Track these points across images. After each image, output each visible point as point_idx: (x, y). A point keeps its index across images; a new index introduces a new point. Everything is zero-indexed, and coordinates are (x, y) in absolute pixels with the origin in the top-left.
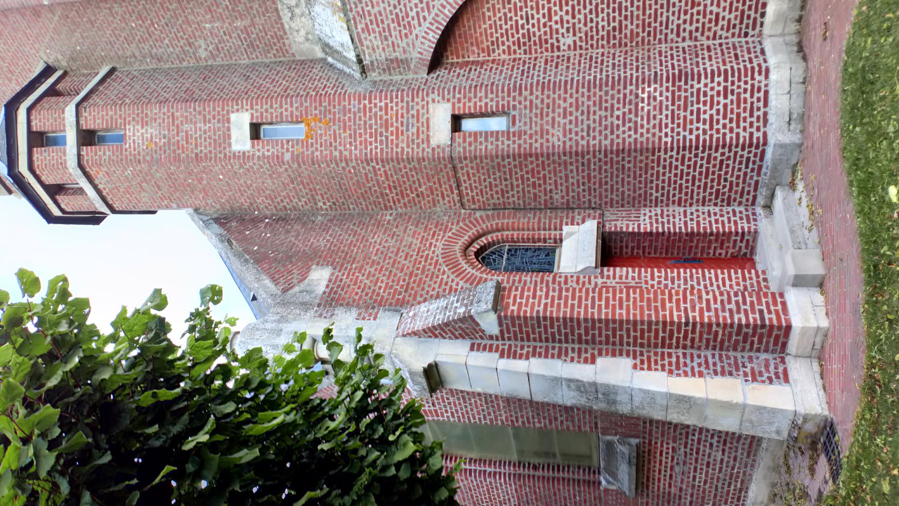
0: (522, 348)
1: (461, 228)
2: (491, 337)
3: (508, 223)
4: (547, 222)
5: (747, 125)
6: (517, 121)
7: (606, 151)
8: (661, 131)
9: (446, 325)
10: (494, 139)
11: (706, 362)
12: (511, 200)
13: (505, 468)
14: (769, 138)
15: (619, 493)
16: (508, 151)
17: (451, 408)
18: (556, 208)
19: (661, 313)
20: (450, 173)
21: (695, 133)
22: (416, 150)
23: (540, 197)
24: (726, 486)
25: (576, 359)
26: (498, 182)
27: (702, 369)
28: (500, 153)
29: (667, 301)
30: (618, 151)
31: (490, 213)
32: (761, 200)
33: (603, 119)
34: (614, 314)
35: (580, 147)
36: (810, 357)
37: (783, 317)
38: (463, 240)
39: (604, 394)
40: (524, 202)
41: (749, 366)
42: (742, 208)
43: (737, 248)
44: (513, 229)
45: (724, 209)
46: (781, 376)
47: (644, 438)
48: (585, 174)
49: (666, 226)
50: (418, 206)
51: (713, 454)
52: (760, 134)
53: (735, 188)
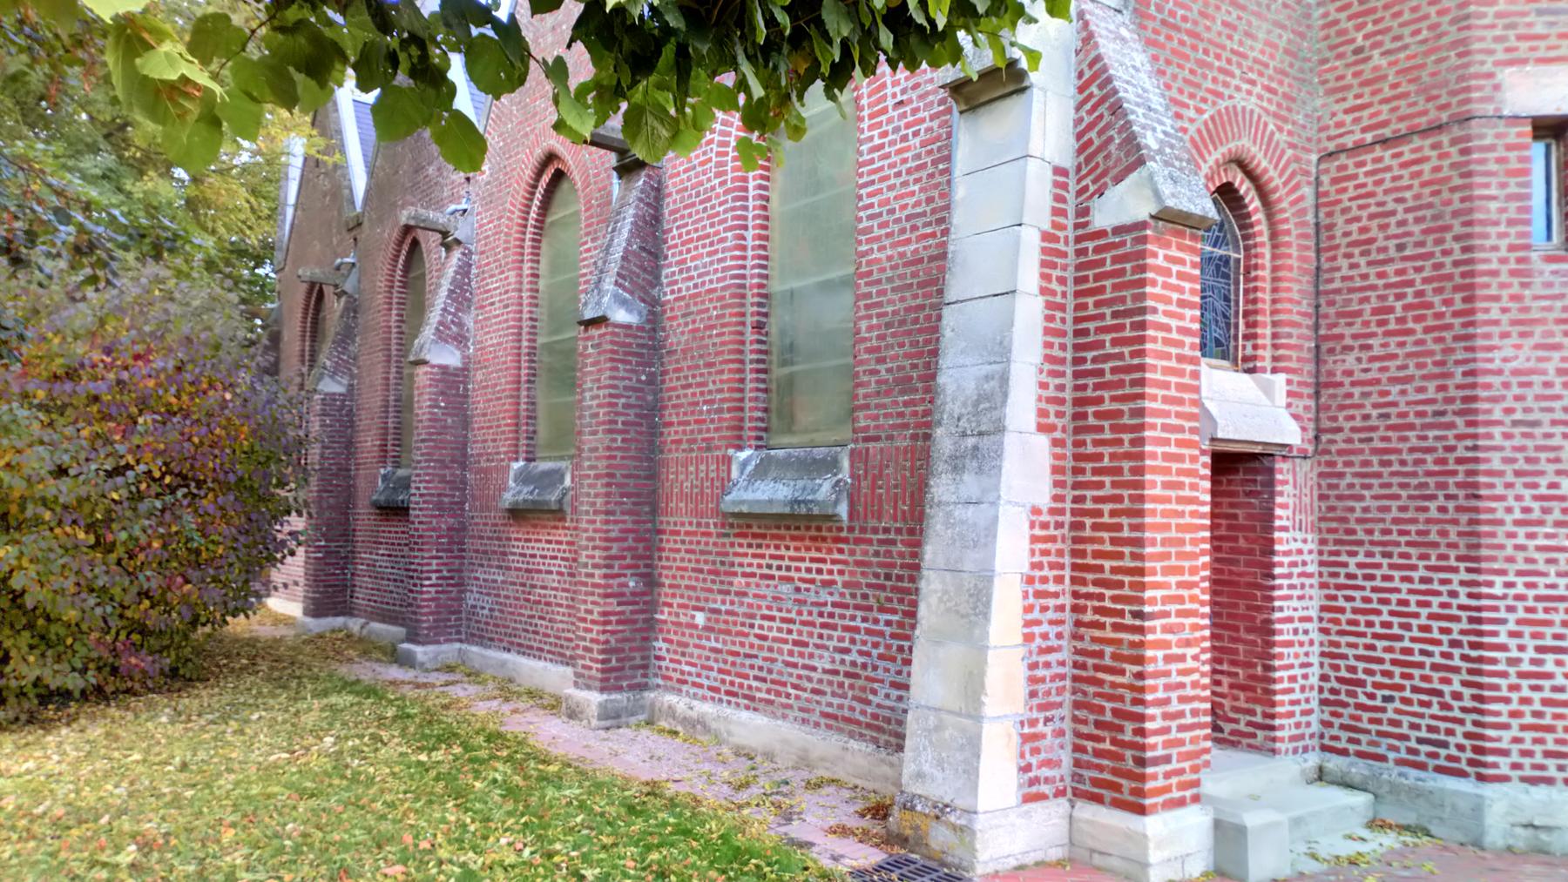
0: (1062, 281)
1: (1283, 152)
2: (1084, 212)
3: (1289, 256)
4: (1293, 341)
5: (1527, 746)
6: (1555, 267)
7: (1476, 460)
8: (1520, 573)
9: (1117, 109)
10: (1513, 215)
11: (1050, 650)
12: (1344, 263)
13: (753, 267)
14: (1497, 786)
15: (725, 485)
16: (1482, 248)
17: (892, 143)
18: (1318, 361)
19: (1158, 565)
20: (1423, 120)
21: (1513, 643)
22: (1490, 34)
23: (1350, 324)
24: (756, 672)
25: (1045, 393)
26: (1393, 230)
27: (1038, 641)
28: (1477, 229)
29: (1179, 578)
30: (1476, 485)
31: (1310, 218)
32: (1334, 763)
33: (1552, 455)
34: (1155, 470)
35: (1486, 406)
36: (1071, 843)
37: (1160, 799)
38: (1260, 155)
39: (976, 448)
40: (1338, 291)
41: (1048, 730)
42: (1316, 727)
43: (1232, 715)
44: (1275, 269)
45: (1315, 693)
46: (1034, 789)
47: (851, 529)
48: (1411, 419)
49: (1285, 582)
50: (1328, 54)
51: (826, 654)
52: (1504, 770)
53: (1366, 716)
